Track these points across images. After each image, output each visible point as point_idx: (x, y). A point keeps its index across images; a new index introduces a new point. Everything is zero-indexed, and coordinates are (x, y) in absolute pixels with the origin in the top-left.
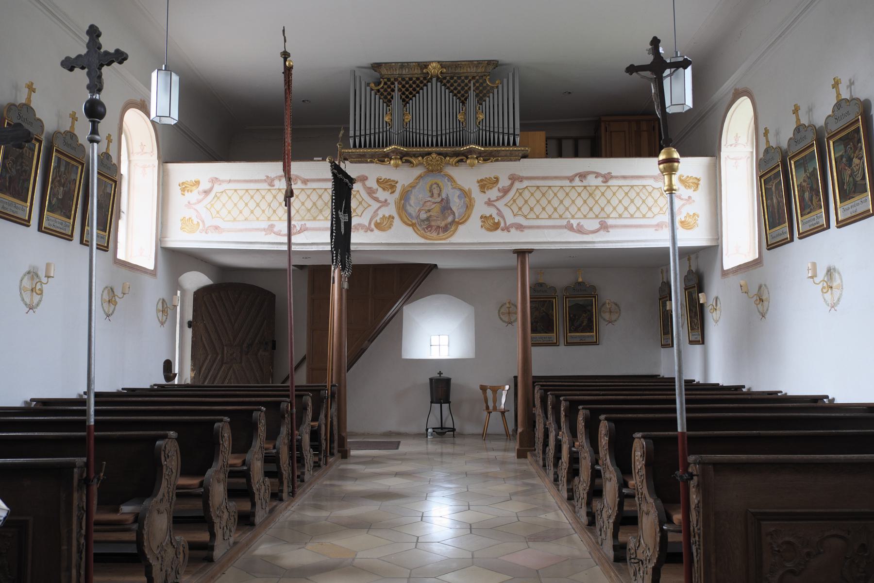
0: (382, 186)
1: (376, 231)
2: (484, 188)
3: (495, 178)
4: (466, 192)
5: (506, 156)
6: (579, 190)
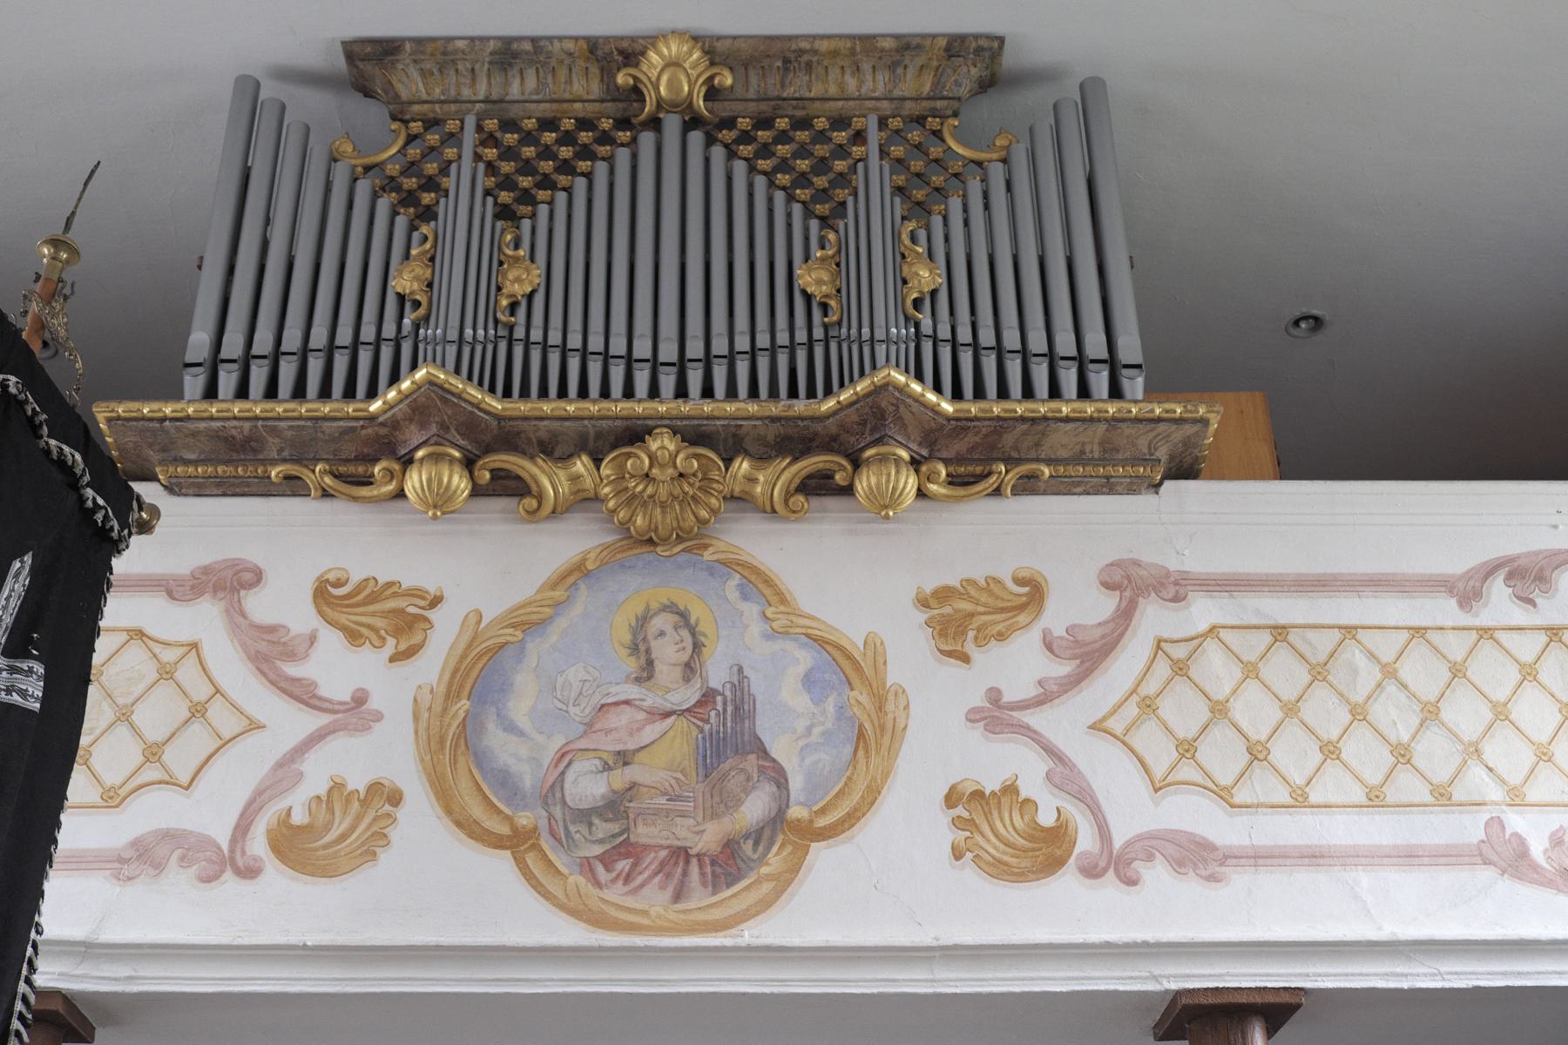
0: (343, 619)
1: (276, 877)
2: (961, 633)
3: (1019, 582)
4: (849, 657)
5: (1080, 458)
6: (1527, 646)
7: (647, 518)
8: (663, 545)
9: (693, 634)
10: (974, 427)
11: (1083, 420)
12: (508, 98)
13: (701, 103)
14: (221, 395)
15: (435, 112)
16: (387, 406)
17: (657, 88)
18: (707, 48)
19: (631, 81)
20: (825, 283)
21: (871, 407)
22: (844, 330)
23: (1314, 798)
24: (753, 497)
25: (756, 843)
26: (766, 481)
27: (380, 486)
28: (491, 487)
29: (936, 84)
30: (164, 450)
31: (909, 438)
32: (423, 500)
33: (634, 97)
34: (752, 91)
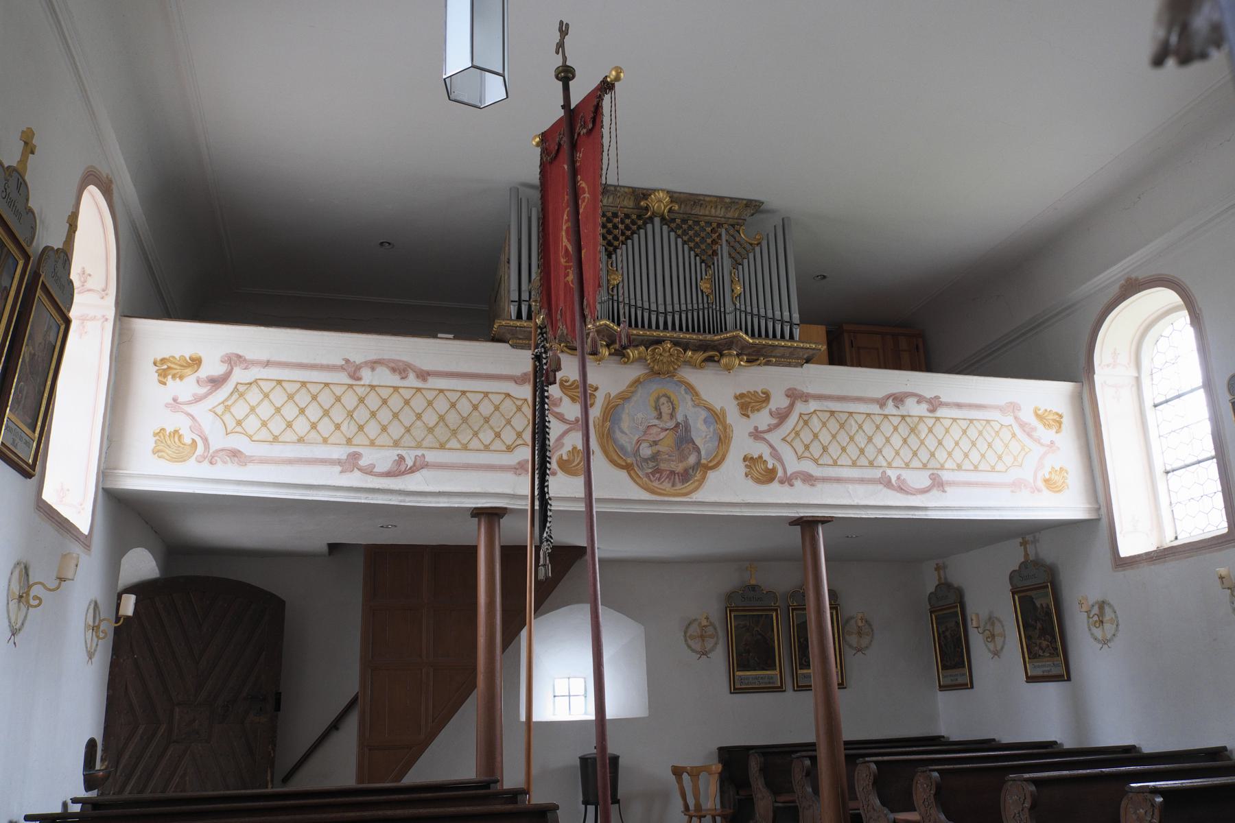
0: (569, 393)
5: (783, 356)
6: (896, 421)
9: (672, 404)
23: (839, 463)
25: (693, 470)
30: (513, 334)
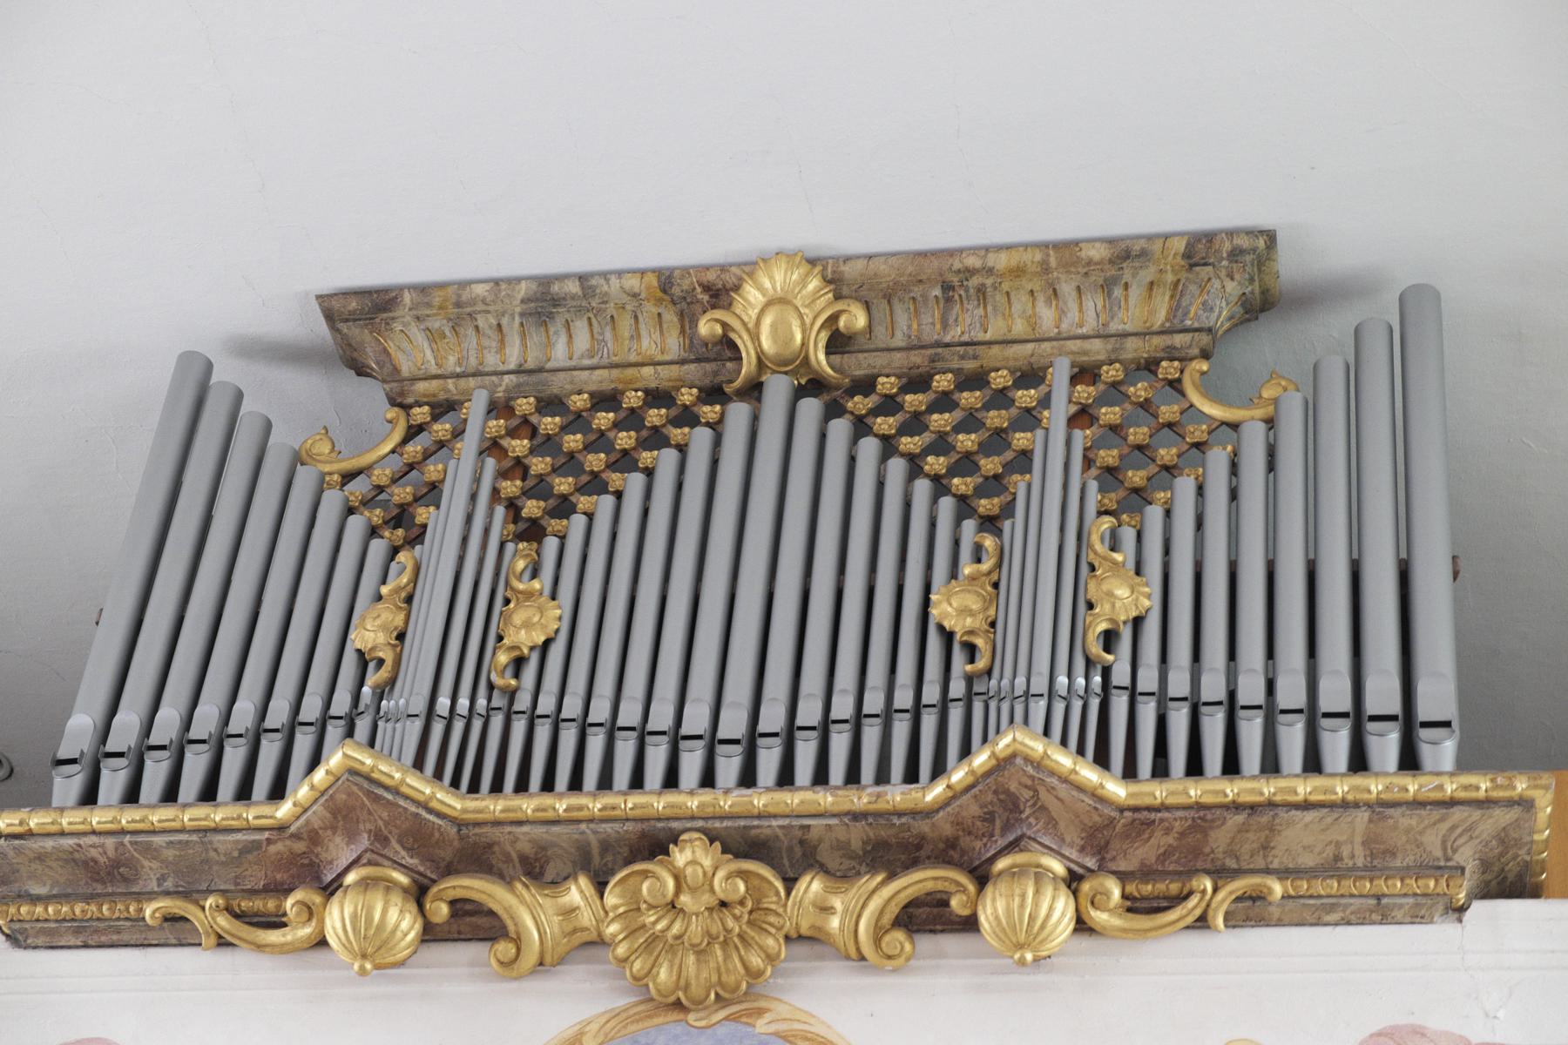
5: (1333, 868)
7: (676, 968)
8: (697, 1011)
10: (1162, 820)
11: (1331, 806)
12: (549, 365)
13: (822, 357)
14: (143, 798)
15: (447, 391)
16: (299, 810)
17: (755, 337)
18: (830, 276)
19: (719, 330)
20: (972, 613)
21: (995, 792)
22: (993, 682)
24: (828, 934)
26: (846, 911)
27: (295, 928)
28: (455, 927)
29: (1175, 309)
31: (1063, 840)
32: (347, 947)
33: (728, 354)
34: (899, 334)
